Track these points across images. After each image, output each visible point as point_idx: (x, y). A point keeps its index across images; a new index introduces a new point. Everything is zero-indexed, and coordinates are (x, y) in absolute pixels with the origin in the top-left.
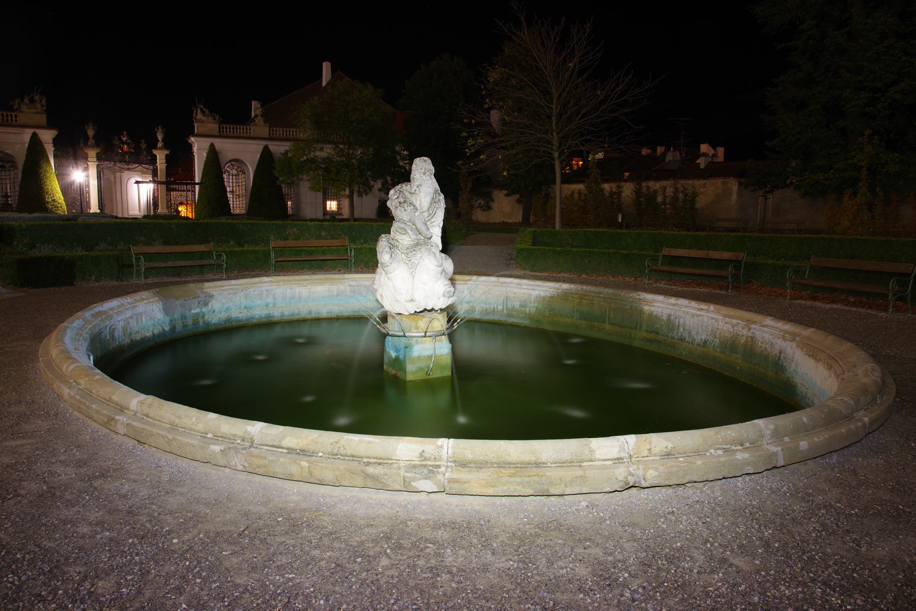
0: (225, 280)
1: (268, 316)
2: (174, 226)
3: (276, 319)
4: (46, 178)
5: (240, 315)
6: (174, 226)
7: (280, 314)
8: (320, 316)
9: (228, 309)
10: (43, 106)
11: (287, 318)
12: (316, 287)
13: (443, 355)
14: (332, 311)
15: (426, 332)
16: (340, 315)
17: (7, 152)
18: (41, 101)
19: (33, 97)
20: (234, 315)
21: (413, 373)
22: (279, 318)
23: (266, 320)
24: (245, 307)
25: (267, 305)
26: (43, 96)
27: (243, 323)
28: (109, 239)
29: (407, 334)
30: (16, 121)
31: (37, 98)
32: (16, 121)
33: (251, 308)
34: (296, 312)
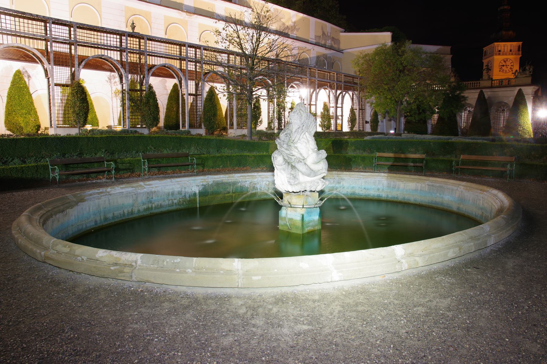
0: (423, 176)
1: (379, 196)
2: (432, 144)
3: (383, 199)
4: (521, 116)
5: (361, 192)
6: (432, 144)
7: (386, 196)
8: (410, 202)
9: (353, 187)
10: (530, 72)
11: (390, 199)
12: (409, 183)
13: (297, 220)
14: (417, 200)
15: (303, 206)
16: (421, 203)
17: (505, 101)
18: (530, 69)
19: (525, 68)
20: (357, 192)
21: (282, 226)
22: (385, 199)
23: (377, 198)
24: (365, 188)
25: (378, 189)
26: (531, 66)
27: (363, 197)
28: (394, 149)
29: (292, 206)
30: (479, 85)
31: (527, 68)
32: (479, 85)
33: (368, 189)
34: (396, 197)
